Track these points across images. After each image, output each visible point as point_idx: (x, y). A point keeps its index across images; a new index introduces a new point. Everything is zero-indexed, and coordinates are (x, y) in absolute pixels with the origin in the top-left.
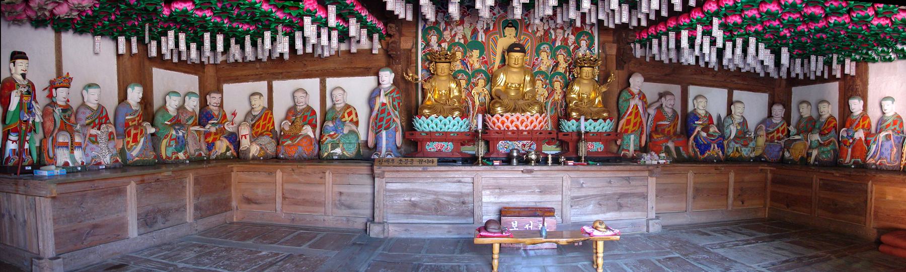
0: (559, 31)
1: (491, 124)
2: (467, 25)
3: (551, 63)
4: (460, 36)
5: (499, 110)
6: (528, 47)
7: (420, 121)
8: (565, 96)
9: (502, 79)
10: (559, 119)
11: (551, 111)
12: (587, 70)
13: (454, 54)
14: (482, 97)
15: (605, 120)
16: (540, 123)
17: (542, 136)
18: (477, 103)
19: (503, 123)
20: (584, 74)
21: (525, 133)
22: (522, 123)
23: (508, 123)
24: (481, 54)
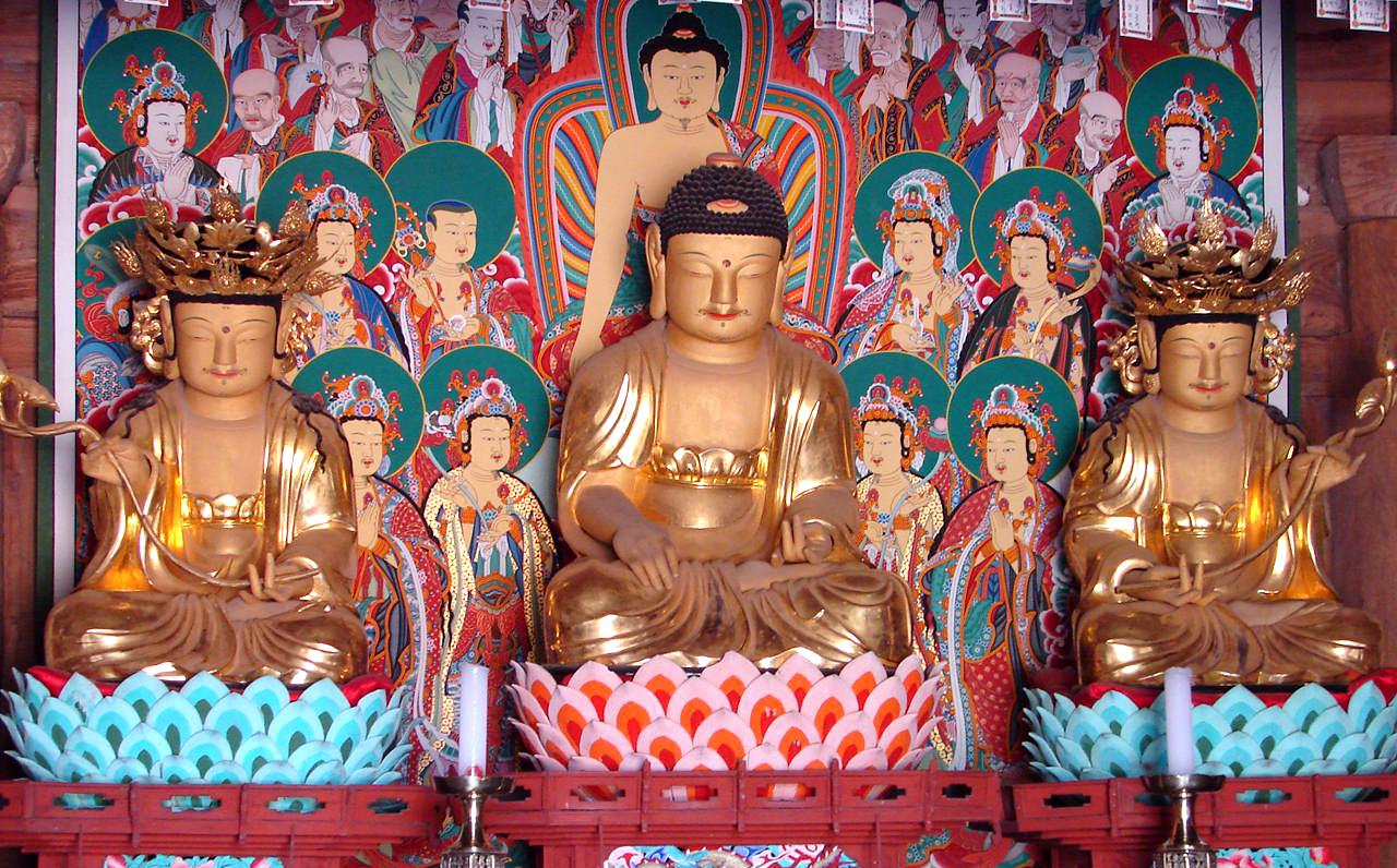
0: (1016, 66)
1: (551, 730)
2: (390, 27)
3: (961, 294)
4: (342, 108)
5: (608, 631)
6: (801, 192)
7: (60, 709)
8: (1057, 529)
9: (625, 422)
10: (1022, 681)
11: (967, 634)
12: (1205, 343)
13: (302, 243)
14: (495, 541)
15: (1340, 688)
16: (885, 720)
17: (892, 811)
18: (463, 582)
19: (633, 724)
20: (1188, 373)
21: (786, 791)
22: (762, 722)
23: (665, 725)
24: (489, 239)
